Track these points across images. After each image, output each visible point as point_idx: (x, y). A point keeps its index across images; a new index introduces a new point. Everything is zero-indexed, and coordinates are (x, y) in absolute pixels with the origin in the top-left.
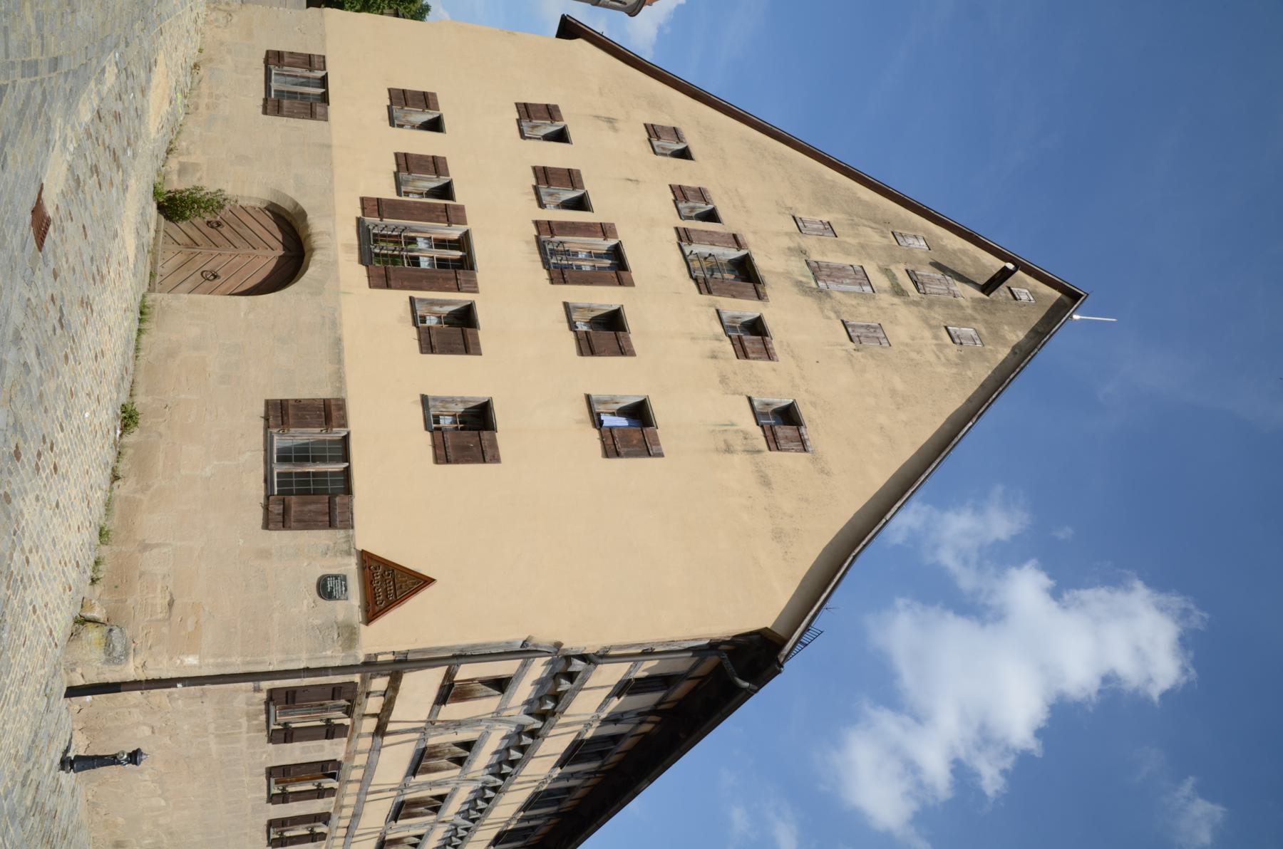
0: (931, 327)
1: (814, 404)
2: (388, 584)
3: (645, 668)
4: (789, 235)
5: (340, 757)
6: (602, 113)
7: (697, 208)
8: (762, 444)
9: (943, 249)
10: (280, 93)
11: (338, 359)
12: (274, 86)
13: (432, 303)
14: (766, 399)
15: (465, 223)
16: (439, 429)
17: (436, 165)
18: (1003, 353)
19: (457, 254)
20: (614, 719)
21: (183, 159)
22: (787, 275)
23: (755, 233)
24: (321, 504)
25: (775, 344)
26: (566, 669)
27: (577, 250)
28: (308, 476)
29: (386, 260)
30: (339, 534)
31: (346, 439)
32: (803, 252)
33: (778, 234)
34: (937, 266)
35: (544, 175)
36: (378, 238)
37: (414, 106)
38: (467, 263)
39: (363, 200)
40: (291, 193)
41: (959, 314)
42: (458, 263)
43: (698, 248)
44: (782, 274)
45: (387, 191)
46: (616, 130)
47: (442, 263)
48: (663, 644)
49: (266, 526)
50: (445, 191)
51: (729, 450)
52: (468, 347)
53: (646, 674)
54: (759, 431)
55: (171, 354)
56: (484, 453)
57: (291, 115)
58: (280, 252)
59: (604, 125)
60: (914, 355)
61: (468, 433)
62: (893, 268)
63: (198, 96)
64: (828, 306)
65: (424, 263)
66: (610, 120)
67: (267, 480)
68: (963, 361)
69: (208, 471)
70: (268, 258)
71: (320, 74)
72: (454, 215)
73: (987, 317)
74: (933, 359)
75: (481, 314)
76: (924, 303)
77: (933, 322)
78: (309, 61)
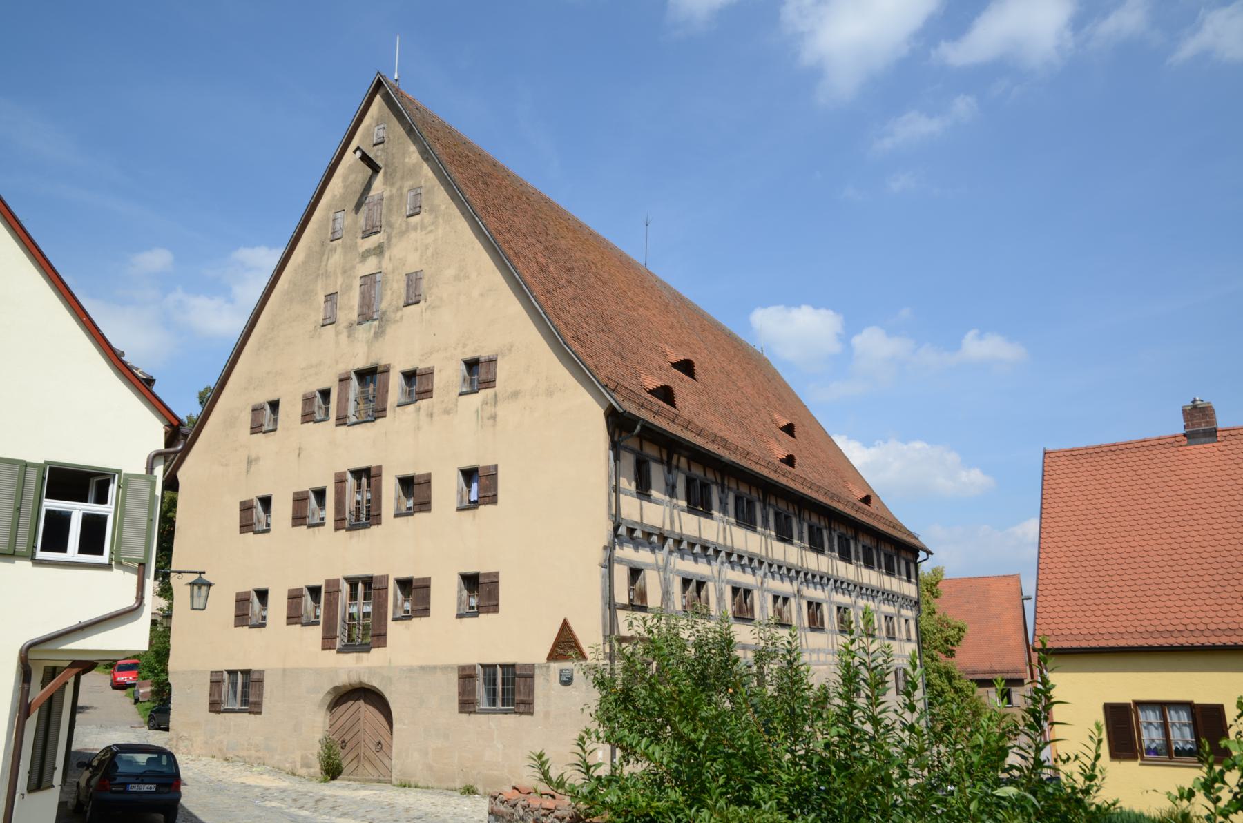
0: (407, 231)
1: (465, 346)
2: (565, 644)
3: (628, 484)
4: (338, 333)
7: (317, 405)
8: (490, 392)
9: (344, 197)
10: (245, 702)
11: (434, 669)
12: (238, 707)
13: (395, 606)
14: (460, 380)
15: (338, 580)
16: (478, 607)
17: (294, 597)
18: (426, 170)
19: (360, 586)
20: (671, 491)
21: (299, 766)
22: (369, 344)
23: (337, 363)
25: (422, 366)
26: (624, 533)
27: (359, 500)
28: (505, 688)
29: (366, 635)
30: (537, 672)
31: (483, 666)
32: (351, 326)
33: (337, 343)
34: (358, 207)
35: (299, 519)
37: (248, 609)
38: (368, 581)
39: (324, 649)
40: (321, 696)
42: (367, 586)
43: (351, 410)
45: (317, 632)
46: (257, 459)
47: (366, 597)
48: (609, 481)
49: (531, 714)
50: (315, 591)
51: (494, 417)
52: (425, 585)
53: (633, 484)
54: (481, 392)
55: (430, 768)
57: (261, 695)
58: (361, 703)
59: (254, 468)
60: (429, 252)
61: (480, 590)
62: (361, 250)
63: (250, 757)
64: (393, 315)
65: (368, 609)
66: (250, 462)
67: (506, 712)
68: (434, 210)
69: (500, 746)
71: (226, 675)
73: (399, 175)
74: (430, 238)
76: (389, 230)
78: (216, 682)
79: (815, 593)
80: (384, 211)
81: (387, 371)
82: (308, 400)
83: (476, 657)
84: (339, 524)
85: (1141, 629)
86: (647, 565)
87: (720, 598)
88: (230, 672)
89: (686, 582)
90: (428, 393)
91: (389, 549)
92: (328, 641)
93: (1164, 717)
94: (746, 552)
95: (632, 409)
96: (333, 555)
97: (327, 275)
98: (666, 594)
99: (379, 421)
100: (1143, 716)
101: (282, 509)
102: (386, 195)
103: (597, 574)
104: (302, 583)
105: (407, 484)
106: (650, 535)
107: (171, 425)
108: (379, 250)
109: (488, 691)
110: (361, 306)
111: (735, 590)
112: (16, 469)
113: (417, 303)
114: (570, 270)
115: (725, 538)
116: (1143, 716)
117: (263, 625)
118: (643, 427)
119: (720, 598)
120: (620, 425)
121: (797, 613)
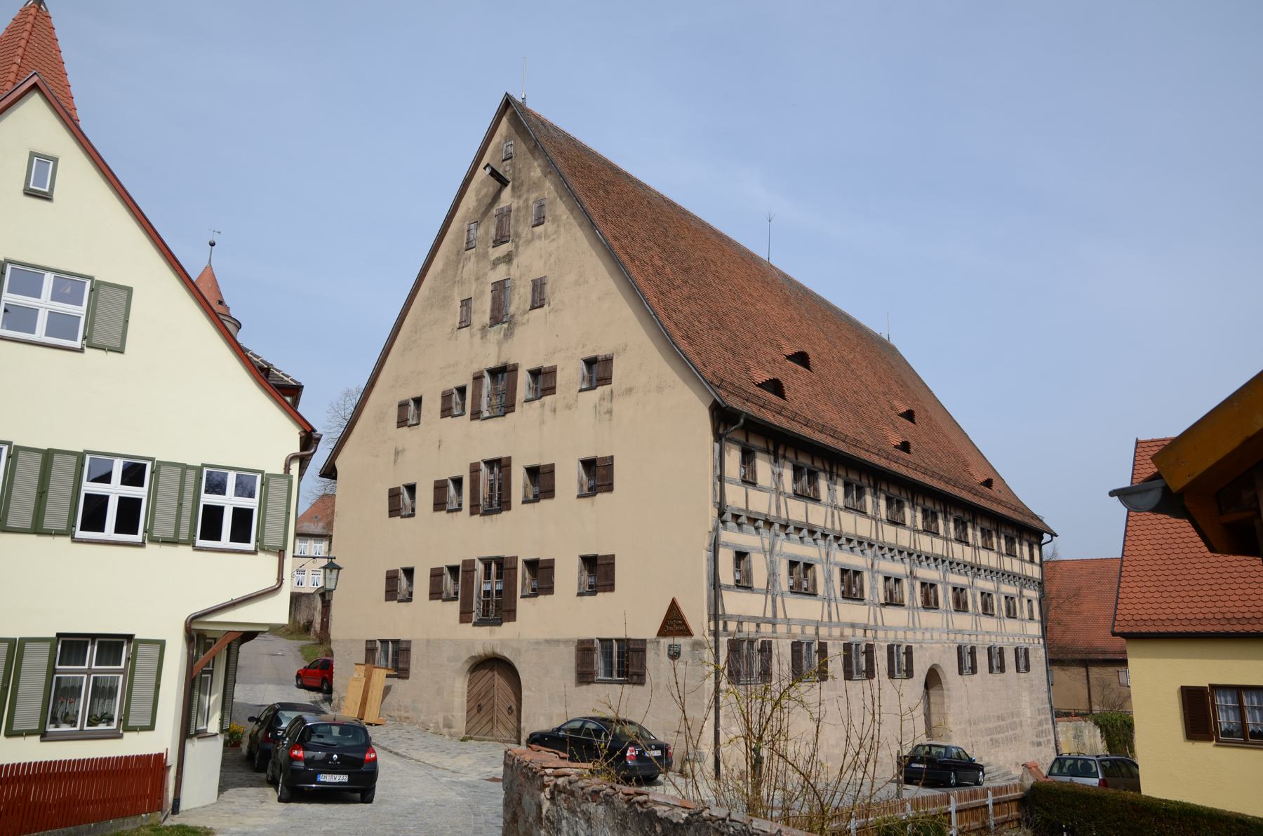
0: (532, 239)
2: (674, 623)
4: (472, 336)
5: (789, 642)
6: (393, 457)
8: (606, 388)
11: (558, 642)
13: (524, 585)
14: (580, 377)
17: (436, 575)
19: (493, 566)
21: (441, 725)
22: (500, 344)
24: (633, 656)
27: (490, 489)
29: (499, 610)
30: (649, 646)
31: (601, 640)
32: (483, 328)
35: (439, 505)
36: (486, 612)
38: (500, 562)
41: (523, 212)
42: (501, 567)
43: (484, 406)
44: (500, 349)
45: (455, 607)
46: (403, 450)
47: (499, 576)
50: (454, 570)
51: (610, 412)
54: (599, 388)
56: (609, 562)
57: (408, 662)
60: (552, 260)
61: (599, 572)
62: (493, 258)
65: (499, 587)
66: (397, 453)
67: (621, 683)
68: (556, 219)
70: (499, 681)
71: (378, 644)
72: (469, 566)
73: (525, 188)
74: (554, 245)
75: (531, 556)
77: (530, 236)
79: (928, 573)
80: (512, 221)
81: (515, 368)
82: (446, 397)
83: (593, 631)
84: (474, 509)
85: (1219, 616)
86: (754, 549)
87: (829, 580)
88: (382, 641)
89: (793, 564)
90: (551, 390)
91: (519, 533)
92: (465, 616)
93: (1240, 701)
94: (856, 535)
95: (735, 403)
96: (470, 538)
97: (462, 282)
98: (772, 575)
99: (508, 416)
100: (1220, 700)
101: (425, 496)
102: (514, 207)
103: (705, 555)
104: (443, 563)
105: (533, 472)
106: (755, 520)
107: (305, 431)
108: (508, 258)
109: (605, 663)
110: (492, 310)
111: (844, 571)
112: (178, 471)
113: (542, 306)
114: (687, 271)
115: (833, 523)
116: (1220, 700)
117: (410, 600)
118: (746, 420)
119: (829, 580)
120: (725, 420)
121: (910, 593)
